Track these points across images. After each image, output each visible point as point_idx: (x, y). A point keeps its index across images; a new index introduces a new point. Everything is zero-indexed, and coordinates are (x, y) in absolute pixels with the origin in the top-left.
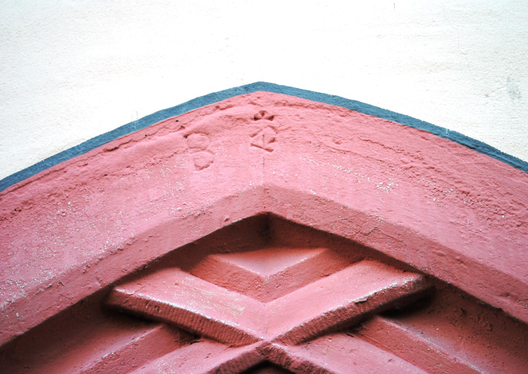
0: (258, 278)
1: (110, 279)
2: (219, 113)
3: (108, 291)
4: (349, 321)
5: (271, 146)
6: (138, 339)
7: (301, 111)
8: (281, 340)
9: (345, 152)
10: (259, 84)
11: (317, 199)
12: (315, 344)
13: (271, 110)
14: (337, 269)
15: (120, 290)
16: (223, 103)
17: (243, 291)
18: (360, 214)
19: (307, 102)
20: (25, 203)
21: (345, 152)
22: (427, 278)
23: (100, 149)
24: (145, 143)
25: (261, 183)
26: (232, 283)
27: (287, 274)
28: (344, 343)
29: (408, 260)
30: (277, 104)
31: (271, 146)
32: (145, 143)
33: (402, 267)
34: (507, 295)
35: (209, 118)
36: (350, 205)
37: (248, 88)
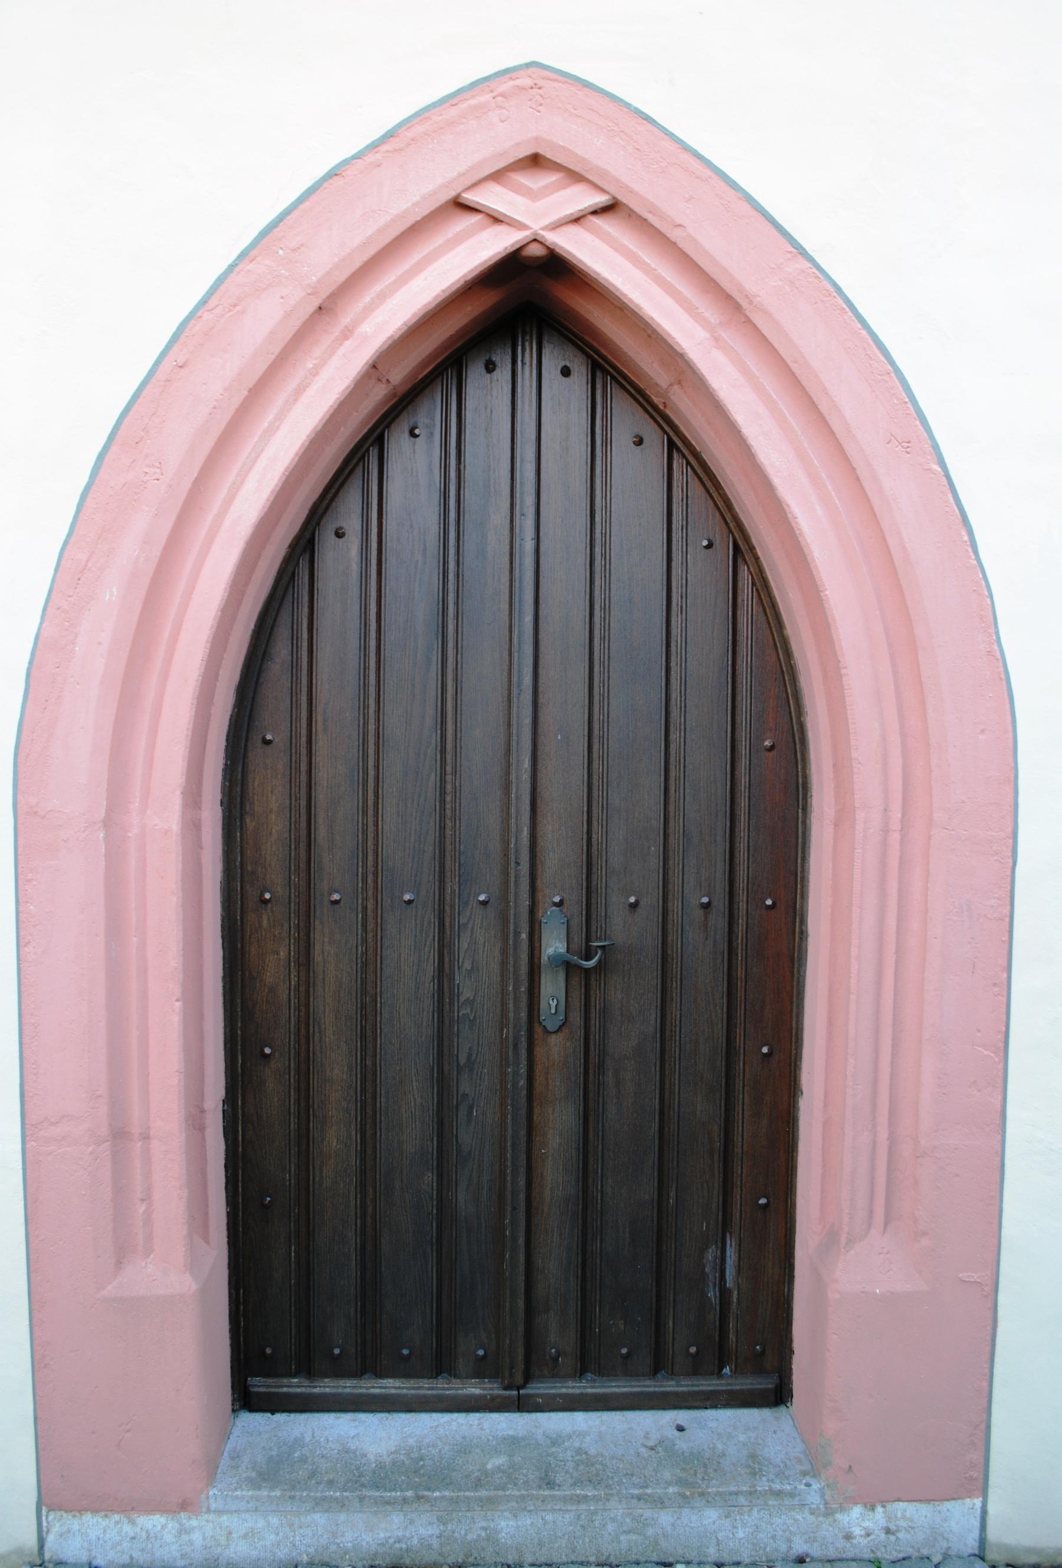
0: (531, 189)
1: (459, 190)
2: (512, 83)
3: (459, 196)
4: (574, 218)
5: (540, 108)
6: (473, 221)
7: (555, 84)
8: (543, 229)
9: (578, 117)
10: (534, 62)
11: (563, 147)
12: (558, 230)
13: (540, 83)
14: (569, 185)
15: (464, 195)
16: (514, 75)
17: (523, 195)
18: (584, 159)
19: (560, 78)
20: (413, 140)
21: (578, 117)
22: (614, 198)
23: (447, 104)
24: (473, 102)
25: (534, 135)
26: (519, 190)
27: (545, 187)
28: (573, 229)
29: (605, 188)
30: (543, 78)
31: (540, 108)
32: (473, 102)
33: (603, 191)
34: (650, 212)
35: (506, 86)
36: (579, 152)
37: (528, 65)
